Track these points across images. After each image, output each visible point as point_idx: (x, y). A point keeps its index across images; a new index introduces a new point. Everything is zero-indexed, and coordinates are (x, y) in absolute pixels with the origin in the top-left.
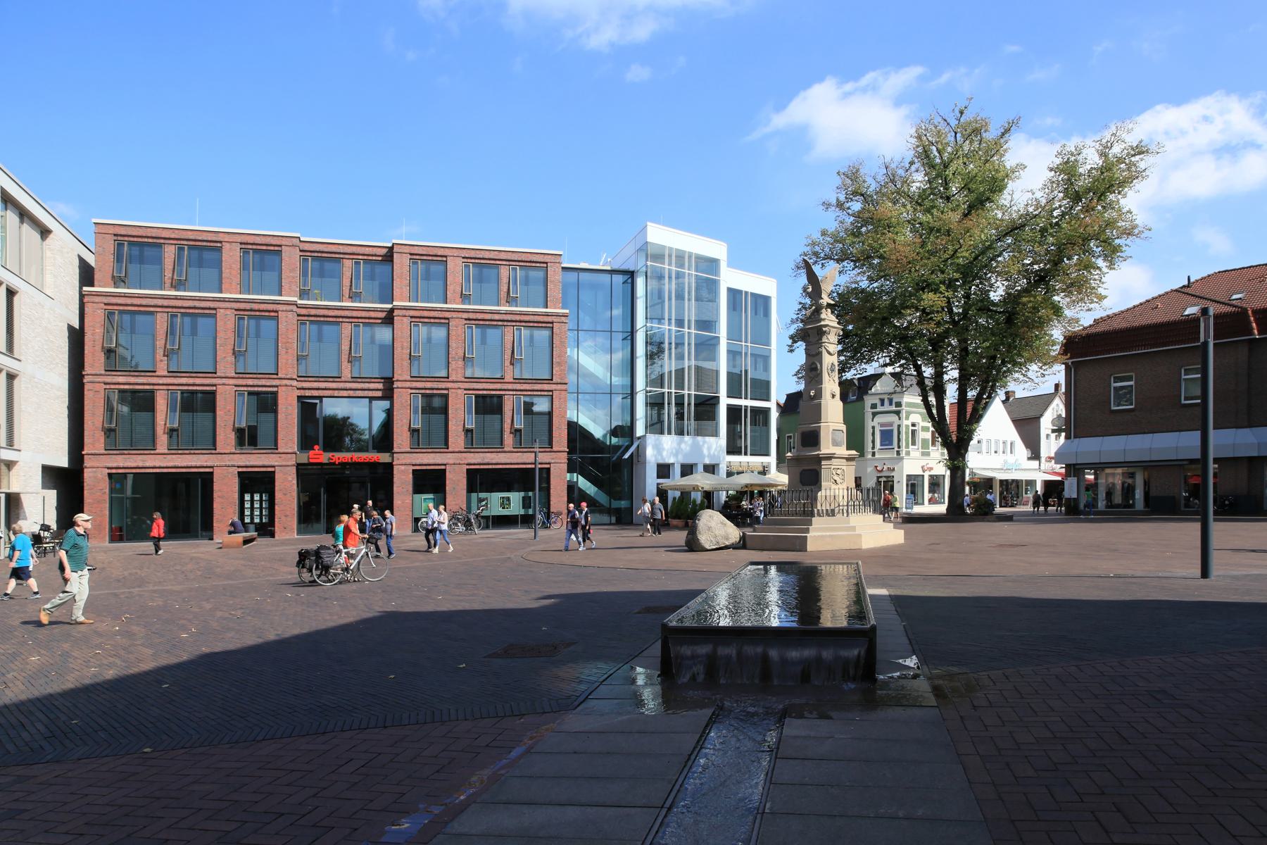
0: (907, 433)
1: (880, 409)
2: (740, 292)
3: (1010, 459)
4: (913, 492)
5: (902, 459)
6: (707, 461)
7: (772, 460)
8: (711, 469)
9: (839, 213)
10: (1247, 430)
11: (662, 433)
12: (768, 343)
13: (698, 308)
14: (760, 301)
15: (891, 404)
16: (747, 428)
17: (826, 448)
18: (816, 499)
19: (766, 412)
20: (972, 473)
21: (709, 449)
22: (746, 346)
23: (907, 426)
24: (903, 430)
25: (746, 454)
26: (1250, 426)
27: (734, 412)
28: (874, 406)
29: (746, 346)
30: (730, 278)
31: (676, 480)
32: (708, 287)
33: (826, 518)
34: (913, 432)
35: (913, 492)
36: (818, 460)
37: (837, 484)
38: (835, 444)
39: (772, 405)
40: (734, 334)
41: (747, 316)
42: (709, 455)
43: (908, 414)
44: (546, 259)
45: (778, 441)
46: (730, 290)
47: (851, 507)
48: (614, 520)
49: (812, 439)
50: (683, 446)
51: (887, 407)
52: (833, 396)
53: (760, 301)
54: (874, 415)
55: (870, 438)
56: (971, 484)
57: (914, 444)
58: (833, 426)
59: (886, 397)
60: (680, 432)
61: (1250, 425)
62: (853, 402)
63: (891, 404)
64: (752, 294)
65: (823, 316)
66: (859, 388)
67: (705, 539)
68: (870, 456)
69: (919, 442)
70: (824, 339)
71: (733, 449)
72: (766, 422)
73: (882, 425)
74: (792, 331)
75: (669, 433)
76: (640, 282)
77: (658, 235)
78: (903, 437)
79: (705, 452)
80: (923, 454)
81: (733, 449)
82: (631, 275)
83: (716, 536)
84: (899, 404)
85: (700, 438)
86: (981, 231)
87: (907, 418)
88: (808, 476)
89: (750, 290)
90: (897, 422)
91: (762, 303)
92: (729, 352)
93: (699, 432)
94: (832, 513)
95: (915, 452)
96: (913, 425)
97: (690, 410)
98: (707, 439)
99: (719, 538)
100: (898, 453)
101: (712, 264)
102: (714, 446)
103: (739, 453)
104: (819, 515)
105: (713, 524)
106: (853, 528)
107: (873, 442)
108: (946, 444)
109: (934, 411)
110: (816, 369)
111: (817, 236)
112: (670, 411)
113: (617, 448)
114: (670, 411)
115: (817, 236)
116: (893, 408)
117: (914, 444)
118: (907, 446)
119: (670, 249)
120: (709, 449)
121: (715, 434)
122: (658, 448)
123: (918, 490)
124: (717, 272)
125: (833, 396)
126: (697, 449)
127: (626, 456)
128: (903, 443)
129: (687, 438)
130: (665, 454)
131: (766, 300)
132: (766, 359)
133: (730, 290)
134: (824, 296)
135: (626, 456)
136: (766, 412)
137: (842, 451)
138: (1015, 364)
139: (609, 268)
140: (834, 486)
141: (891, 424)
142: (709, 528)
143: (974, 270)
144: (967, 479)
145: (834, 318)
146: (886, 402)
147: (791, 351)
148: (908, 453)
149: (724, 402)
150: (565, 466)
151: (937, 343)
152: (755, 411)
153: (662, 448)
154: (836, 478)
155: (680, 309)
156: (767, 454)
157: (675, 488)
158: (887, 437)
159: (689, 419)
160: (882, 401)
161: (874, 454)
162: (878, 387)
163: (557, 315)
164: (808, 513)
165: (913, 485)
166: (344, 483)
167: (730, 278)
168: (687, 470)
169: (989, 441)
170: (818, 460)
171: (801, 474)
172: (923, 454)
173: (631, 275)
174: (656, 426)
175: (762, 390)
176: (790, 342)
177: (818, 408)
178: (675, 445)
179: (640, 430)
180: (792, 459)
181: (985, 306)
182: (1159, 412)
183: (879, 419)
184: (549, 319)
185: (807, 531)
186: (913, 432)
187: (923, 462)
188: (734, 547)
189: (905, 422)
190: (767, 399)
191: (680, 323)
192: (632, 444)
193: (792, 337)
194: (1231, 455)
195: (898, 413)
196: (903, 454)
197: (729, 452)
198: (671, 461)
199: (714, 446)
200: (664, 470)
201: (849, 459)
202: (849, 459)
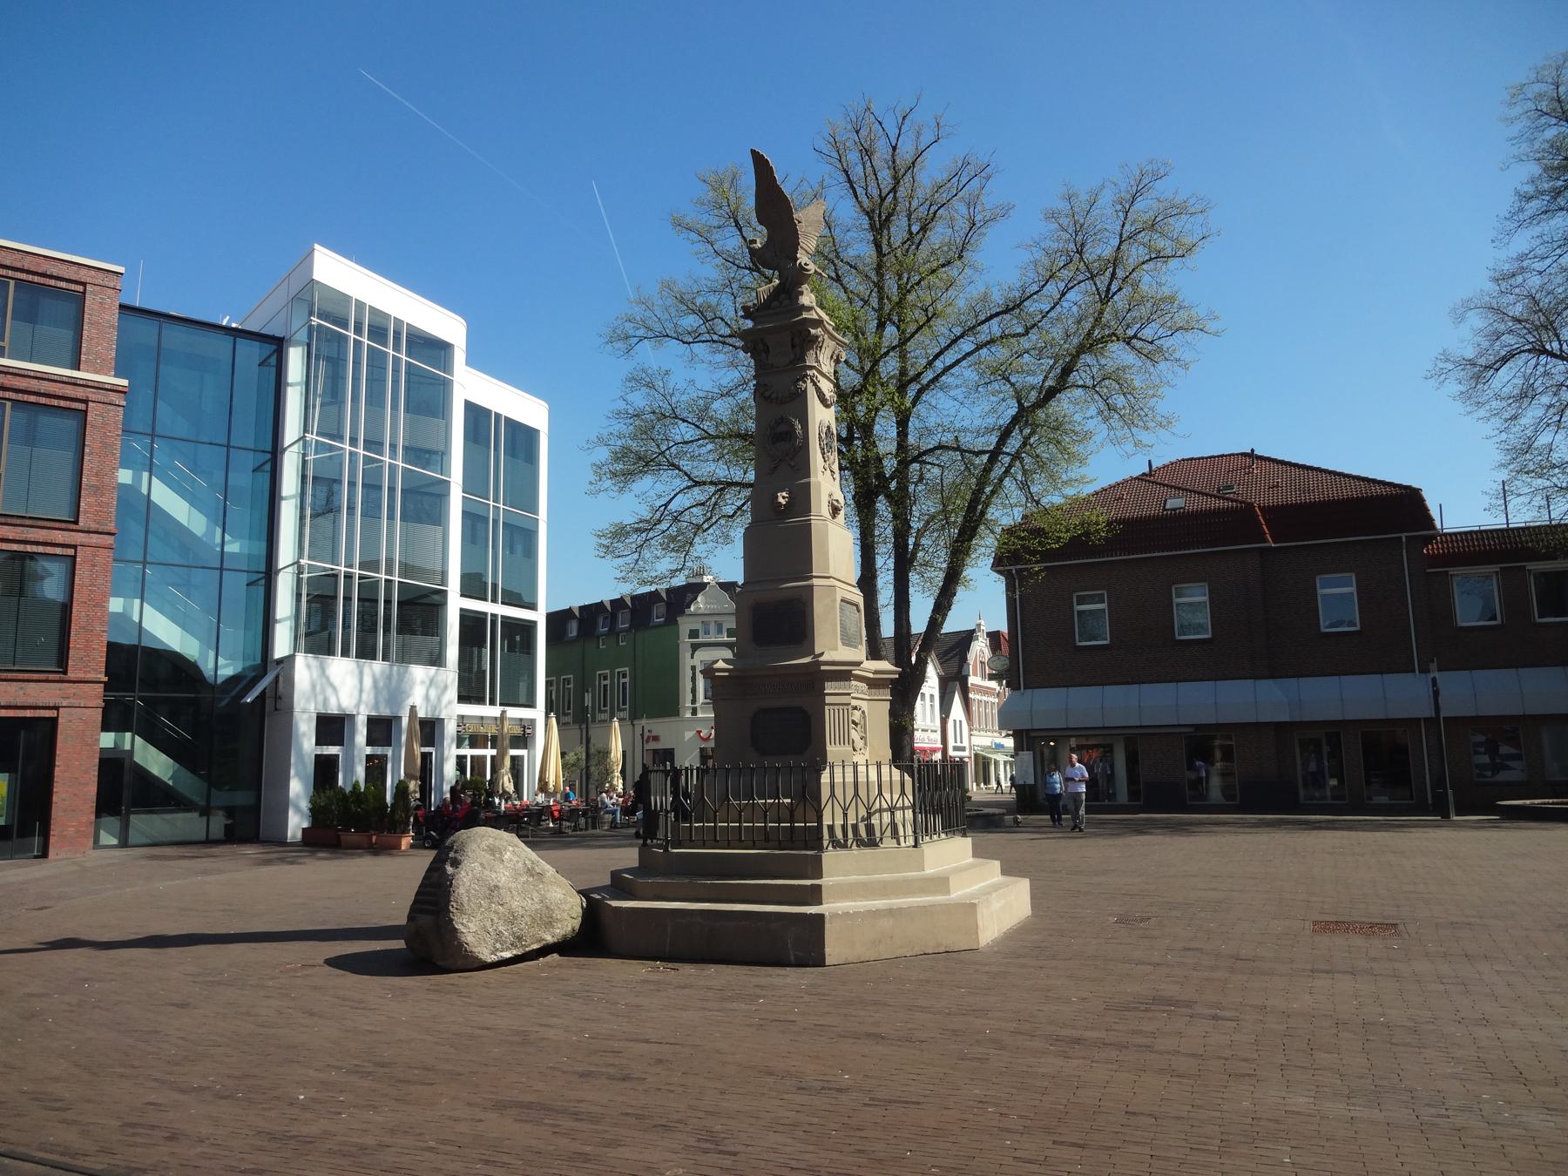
10: (1270, 682)
11: (330, 652)
12: (536, 512)
13: (410, 427)
15: (720, 631)
19: (530, 627)
22: (497, 507)
26: (1272, 677)
27: (472, 626)
28: (694, 634)
29: (497, 507)
30: (470, 385)
32: (429, 397)
33: (856, 852)
39: (539, 617)
40: (475, 481)
41: (498, 459)
44: (83, 275)
46: (470, 407)
54: (695, 647)
55: (689, 685)
60: (366, 652)
61: (1273, 674)
62: (659, 625)
63: (720, 631)
64: (510, 422)
67: (477, 930)
68: (688, 715)
71: (470, 691)
72: (529, 647)
75: (345, 653)
76: (295, 360)
77: (333, 270)
83: (512, 919)
91: (522, 439)
92: (465, 514)
93: (406, 658)
99: (523, 926)
101: (433, 348)
103: (480, 700)
104: (837, 844)
105: (502, 876)
107: (694, 691)
110: (790, 434)
112: (347, 615)
114: (347, 615)
119: (398, 322)
121: (437, 660)
124: (447, 366)
125: (835, 511)
126: (394, 691)
129: (378, 666)
133: (470, 407)
146: (713, 628)
149: (456, 604)
150: (98, 715)
152: (508, 623)
155: (375, 422)
156: (531, 704)
161: (694, 712)
162: (701, 603)
163: (99, 387)
164: (801, 844)
173: (278, 345)
174: (319, 640)
177: (805, 532)
182: (1148, 652)
184: (80, 393)
185: (815, 895)
188: (564, 947)
190: (532, 606)
191: (373, 444)
194: (1381, 715)
197: (463, 699)
199: (431, 689)
200: (332, 727)
202: (873, 684)
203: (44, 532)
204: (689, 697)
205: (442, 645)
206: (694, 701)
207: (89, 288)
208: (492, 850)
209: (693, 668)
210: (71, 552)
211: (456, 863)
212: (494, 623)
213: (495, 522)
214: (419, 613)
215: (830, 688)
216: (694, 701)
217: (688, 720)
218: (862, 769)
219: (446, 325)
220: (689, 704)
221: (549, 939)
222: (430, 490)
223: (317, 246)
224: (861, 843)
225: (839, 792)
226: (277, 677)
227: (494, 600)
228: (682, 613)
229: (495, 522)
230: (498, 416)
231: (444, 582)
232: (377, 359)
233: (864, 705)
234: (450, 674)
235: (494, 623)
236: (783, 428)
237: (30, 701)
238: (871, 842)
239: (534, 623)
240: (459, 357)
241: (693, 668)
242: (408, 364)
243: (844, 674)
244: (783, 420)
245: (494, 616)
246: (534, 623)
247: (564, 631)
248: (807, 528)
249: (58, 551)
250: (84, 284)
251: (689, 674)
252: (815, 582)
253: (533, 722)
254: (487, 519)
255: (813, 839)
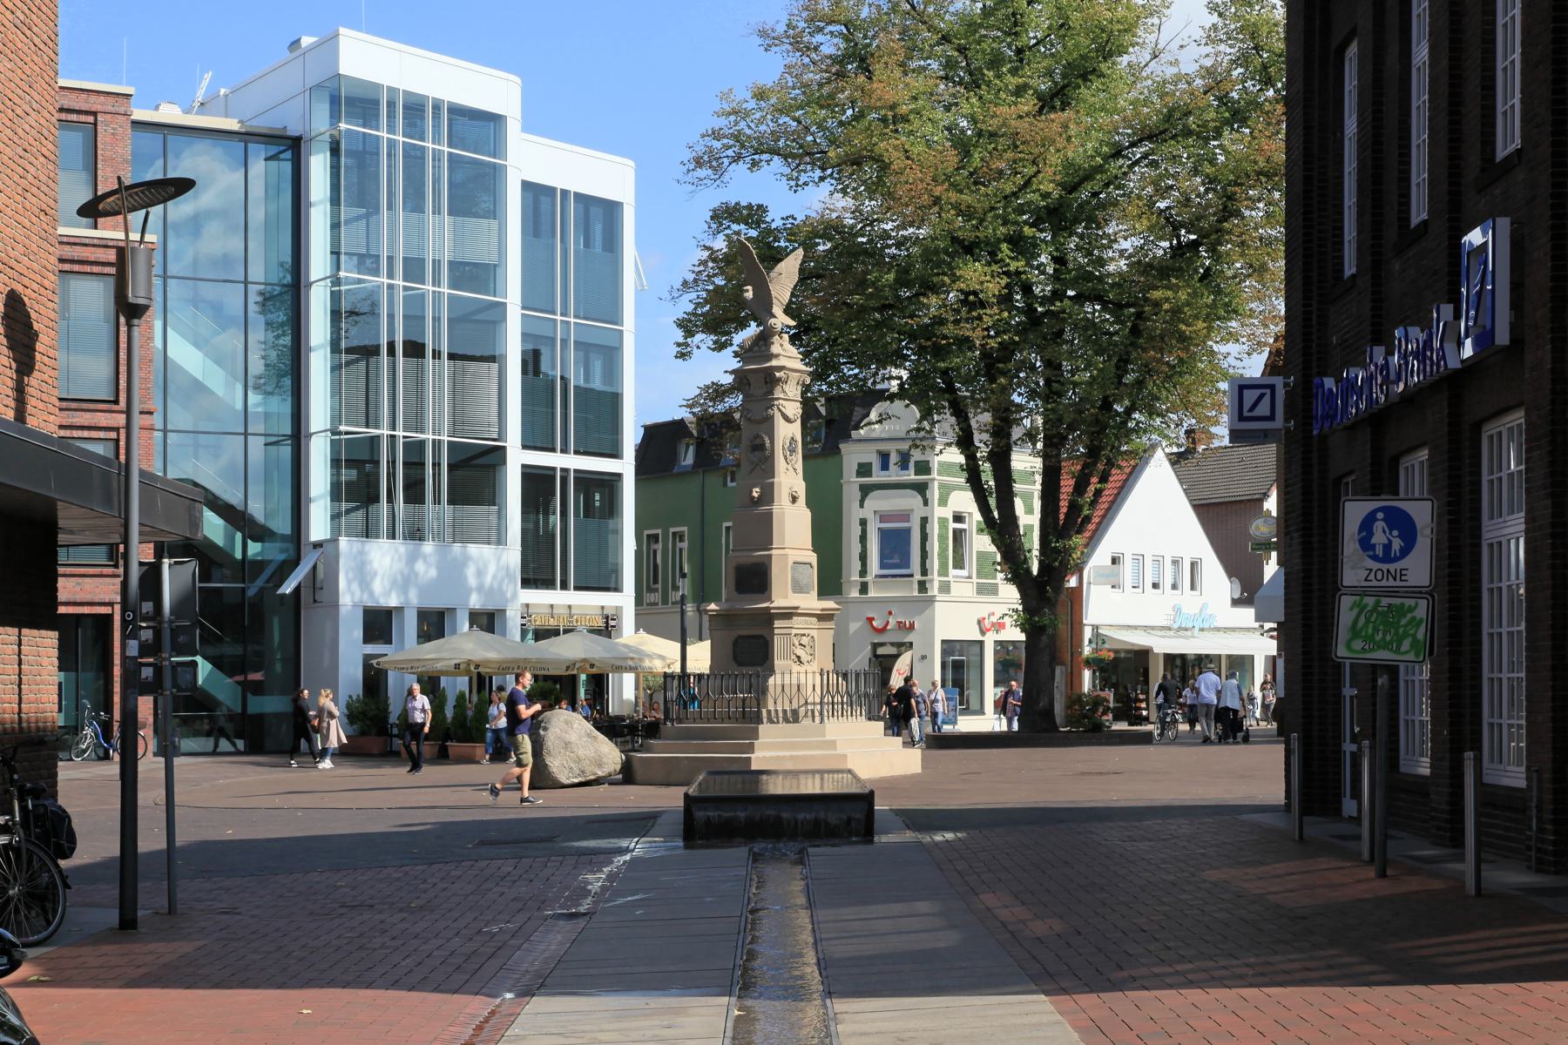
0: (943, 539)
1: (878, 477)
2: (550, 191)
3: (1188, 601)
4: (959, 683)
5: (932, 600)
6: (475, 602)
7: (624, 601)
8: (487, 621)
9: (794, 58)
12: (616, 318)
14: (596, 212)
15: (904, 465)
16: (564, 521)
17: (782, 596)
18: (763, 691)
20: (1098, 637)
21: (480, 573)
22: (567, 322)
23: (943, 521)
24: (935, 530)
25: (564, 586)
27: (538, 484)
28: (864, 470)
30: (530, 159)
31: (407, 647)
32: (475, 190)
33: (782, 725)
34: (958, 536)
35: (959, 683)
36: (768, 618)
37: (803, 664)
38: (798, 588)
42: (480, 588)
43: (946, 491)
44: (94, 104)
45: (638, 554)
46: (527, 186)
47: (829, 707)
48: (240, 744)
49: (755, 579)
50: (420, 566)
51: (894, 475)
52: (794, 499)
53: (596, 212)
54: (866, 490)
55: (856, 548)
56: (1096, 664)
57: (959, 564)
58: (794, 556)
59: (892, 448)
60: (416, 534)
63: (904, 465)
65: (775, 349)
66: (829, 422)
67: (559, 766)
68: (855, 594)
69: (972, 562)
70: (778, 393)
71: (536, 574)
72: (612, 508)
73: (884, 517)
74: (685, 305)
75: (392, 535)
76: (318, 168)
77: (366, 58)
78: (935, 546)
79: (472, 581)
80: (981, 590)
81: (536, 574)
82: (292, 147)
83: (578, 760)
84: (923, 468)
85: (457, 547)
86: (1076, 137)
87: (943, 502)
88: (749, 649)
89: (574, 187)
90: (919, 512)
91: (600, 216)
93: (461, 534)
94: (794, 717)
95: (962, 584)
96: (958, 518)
97: (438, 477)
98: (473, 549)
100: (922, 586)
101: (477, 126)
102: (492, 564)
103: (548, 584)
104: (771, 721)
105: (572, 737)
106: (832, 744)
107: (863, 557)
108: (1018, 574)
109: (992, 502)
110: (762, 447)
111: (743, 95)
113: (258, 566)
115: (743, 95)
116: (911, 476)
117: (959, 564)
118: (943, 571)
119: (392, 90)
120: (480, 573)
121: (500, 540)
122: (363, 576)
123: (970, 676)
124: (498, 148)
125: (794, 499)
126: (452, 572)
127: (288, 588)
128: (935, 563)
130: (378, 586)
131: (611, 210)
132: (611, 354)
133: (527, 186)
134: (777, 310)
135: (288, 588)
136: (610, 483)
137: (811, 602)
138: (1152, 412)
139: (232, 124)
140: (796, 668)
141: (905, 516)
142: (567, 745)
143: (1072, 209)
144: (1087, 651)
145: (793, 351)
147: (682, 356)
148: (945, 588)
149: (518, 457)
151: (994, 364)
152: (587, 482)
153: (376, 569)
154: (800, 652)
157: (401, 667)
158: (896, 546)
159: (437, 501)
160: (884, 458)
161: (864, 588)
164: (750, 718)
165: (958, 666)
166: (592, 666)
167: (530, 159)
168: (434, 624)
169: (1139, 558)
170: (768, 618)
171: (736, 643)
172: (981, 590)
173: (292, 147)
175: (598, 418)
176: (679, 335)
177: (767, 520)
178: (400, 566)
179: (318, 526)
180: (715, 618)
181: (1092, 287)
183: (876, 502)
185: (751, 748)
186: (958, 536)
187: (983, 610)
189: (940, 512)
191: (414, 269)
192: (296, 562)
193: (681, 324)
195: (921, 488)
196: (934, 590)
197: (527, 583)
198: (393, 601)
200: (378, 624)
201: (824, 617)
203: (88, 415)
204: (857, 566)
205: (502, 515)
206: (863, 573)
207: (100, 118)
208: (567, 722)
209: (863, 523)
210: (113, 435)
211: (545, 729)
212: (564, 480)
213: (565, 342)
214: (474, 472)
215: (777, 624)
216: (863, 573)
217: (855, 601)
218: (802, 677)
219: (490, 88)
220: (855, 577)
221: (600, 774)
222: (479, 317)
223: (342, 30)
224: (786, 720)
225: (787, 689)
226: (315, 567)
227: (564, 451)
228: (847, 437)
229: (565, 342)
230: (565, 193)
231: (502, 435)
232: (415, 158)
233: (814, 633)
234: (512, 554)
235: (564, 480)
236: (758, 442)
237: (88, 598)
238: (796, 720)
239: (617, 477)
240: (513, 129)
241: (863, 523)
242: (450, 154)
243: (788, 614)
244: (758, 436)
245: (565, 471)
246: (619, 476)
247: (673, 457)
248: (769, 515)
249: (102, 434)
250: (95, 114)
251: (857, 530)
252: (774, 552)
253: (619, 609)
254: (553, 339)
255: (758, 719)
